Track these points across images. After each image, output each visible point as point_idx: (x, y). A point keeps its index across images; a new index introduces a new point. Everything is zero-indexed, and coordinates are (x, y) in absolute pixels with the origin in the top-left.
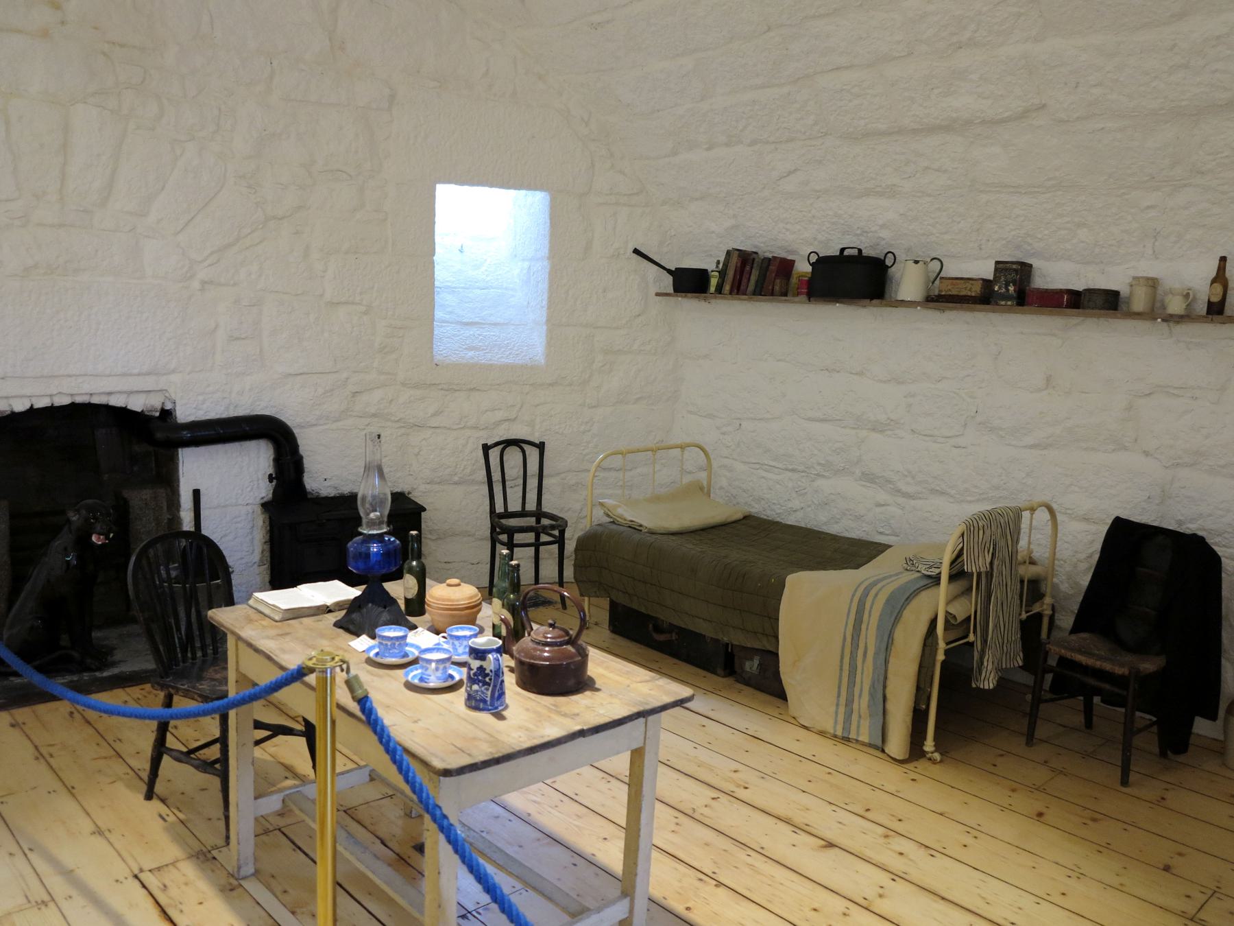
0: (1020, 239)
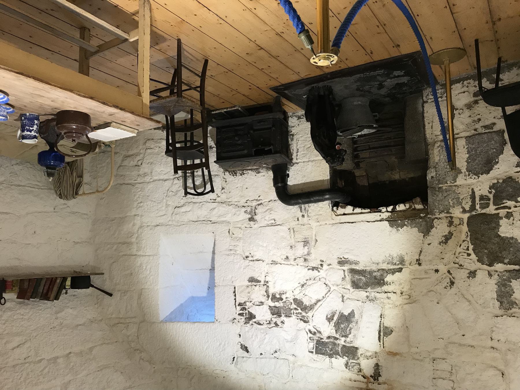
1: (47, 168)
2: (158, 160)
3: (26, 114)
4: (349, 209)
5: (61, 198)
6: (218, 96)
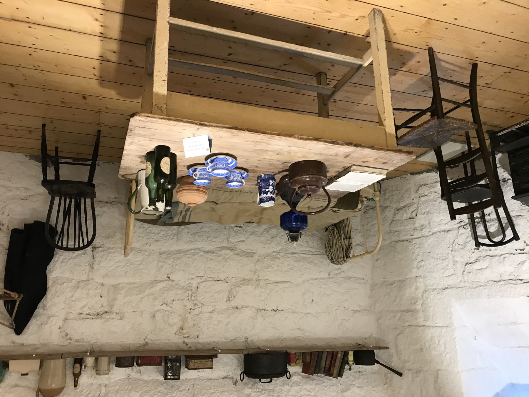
0: (170, 392)
1: (291, 231)
2: (435, 208)
3: (261, 176)
5: (333, 262)
6: (502, 110)
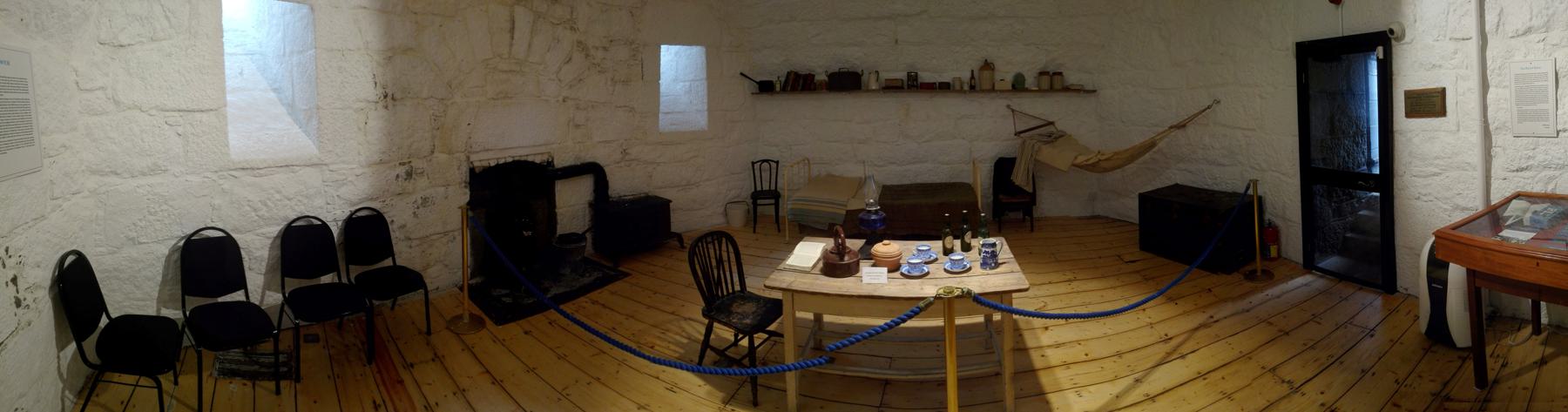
4: (538, 160)
